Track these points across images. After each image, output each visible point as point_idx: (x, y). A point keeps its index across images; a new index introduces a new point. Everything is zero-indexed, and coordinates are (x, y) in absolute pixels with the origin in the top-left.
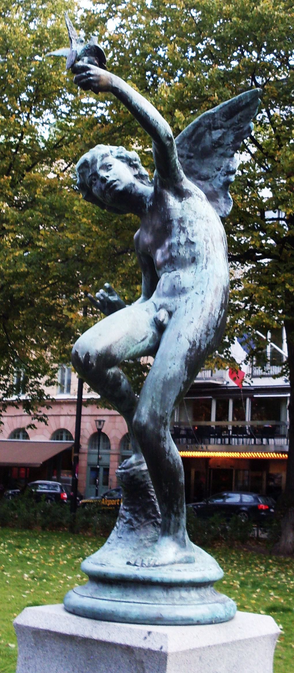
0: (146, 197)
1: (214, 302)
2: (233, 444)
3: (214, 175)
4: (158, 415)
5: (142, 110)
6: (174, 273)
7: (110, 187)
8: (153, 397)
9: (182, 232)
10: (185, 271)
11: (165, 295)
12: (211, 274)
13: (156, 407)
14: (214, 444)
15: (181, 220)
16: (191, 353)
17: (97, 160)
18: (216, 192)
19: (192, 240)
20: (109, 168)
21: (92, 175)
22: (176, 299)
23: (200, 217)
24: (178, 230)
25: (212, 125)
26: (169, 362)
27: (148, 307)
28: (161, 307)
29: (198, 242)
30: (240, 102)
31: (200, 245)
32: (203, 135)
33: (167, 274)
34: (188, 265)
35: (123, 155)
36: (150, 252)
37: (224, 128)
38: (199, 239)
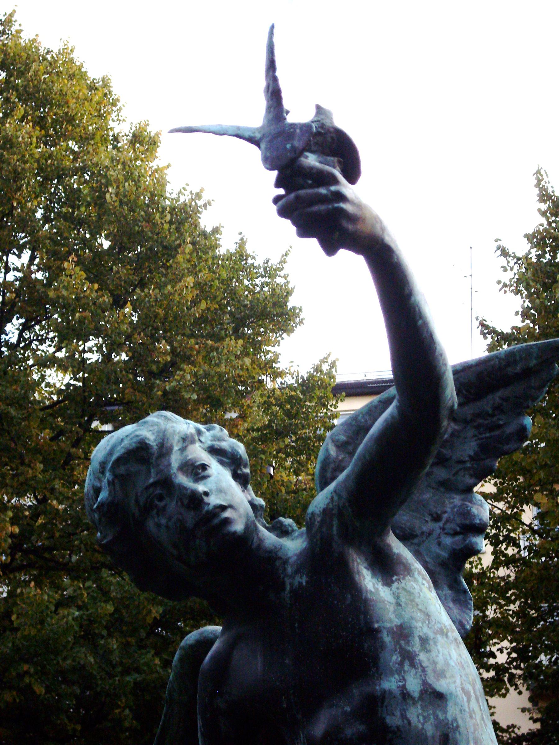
0: (285, 562)
5: (426, 324)
17: (171, 449)
19: (441, 686)
21: (154, 484)
24: (396, 658)
29: (451, 694)
30: (508, 364)
31: (456, 704)
38: (452, 687)
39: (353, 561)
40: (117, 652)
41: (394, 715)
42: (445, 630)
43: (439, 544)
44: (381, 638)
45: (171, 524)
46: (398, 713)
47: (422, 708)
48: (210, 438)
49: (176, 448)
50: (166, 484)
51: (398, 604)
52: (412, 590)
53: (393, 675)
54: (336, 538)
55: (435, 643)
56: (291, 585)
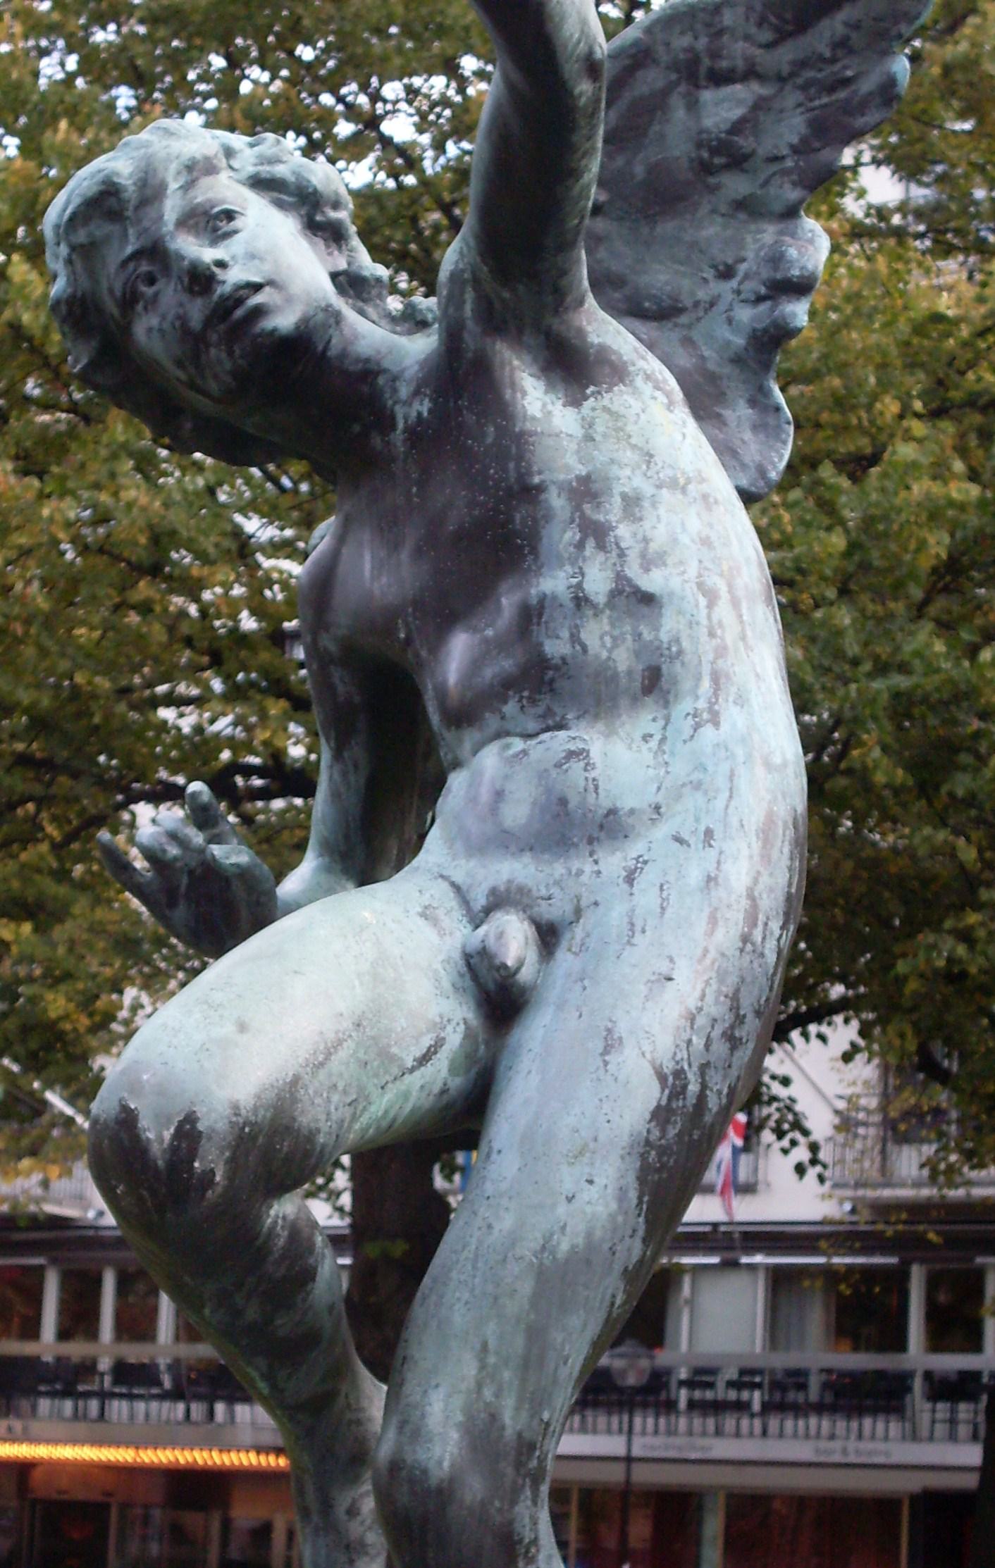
1: (761, 887)
2: (115, 1417)
3: (702, 294)
4: (509, 1433)
6: (558, 741)
7: (230, 314)
8: (484, 1348)
9: (590, 544)
10: (609, 734)
11: (505, 841)
12: (740, 752)
13: (497, 1395)
14: (51, 1416)
15: (586, 491)
16: (663, 1132)
18: (713, 378)
19: (651, 582)
20: (225, 227)
21: (136, 255)
22: (575, 865)
23: (662, 480)
24: (572, 535)
25: (706, 62)
26: (565, 1169)
27: (426, 900)
28: (499, 901)
29: (671, 594)
31: (680, 612)
32: (655, 105)
33: (518, 744)
34: (624, 702)
35: (281, 171)
36: (408, 641)
37: (761, 78)
38: (675, 583)
39: (503, 365)
40: (851, 632)
41: (558, 637)
42: (682, 481)
43: (730, 321)
44: (546, 501)
45: (166, 326)
46: (565, 634)
47: (612, 625)
48: (253, 160)
49: (173, 186)
50: (156, 253)
51: (589, 438)
52: (622, 411)
53: (561, 566)
54: (470, 324)
55: (654, 505)
56: (406, 418)
